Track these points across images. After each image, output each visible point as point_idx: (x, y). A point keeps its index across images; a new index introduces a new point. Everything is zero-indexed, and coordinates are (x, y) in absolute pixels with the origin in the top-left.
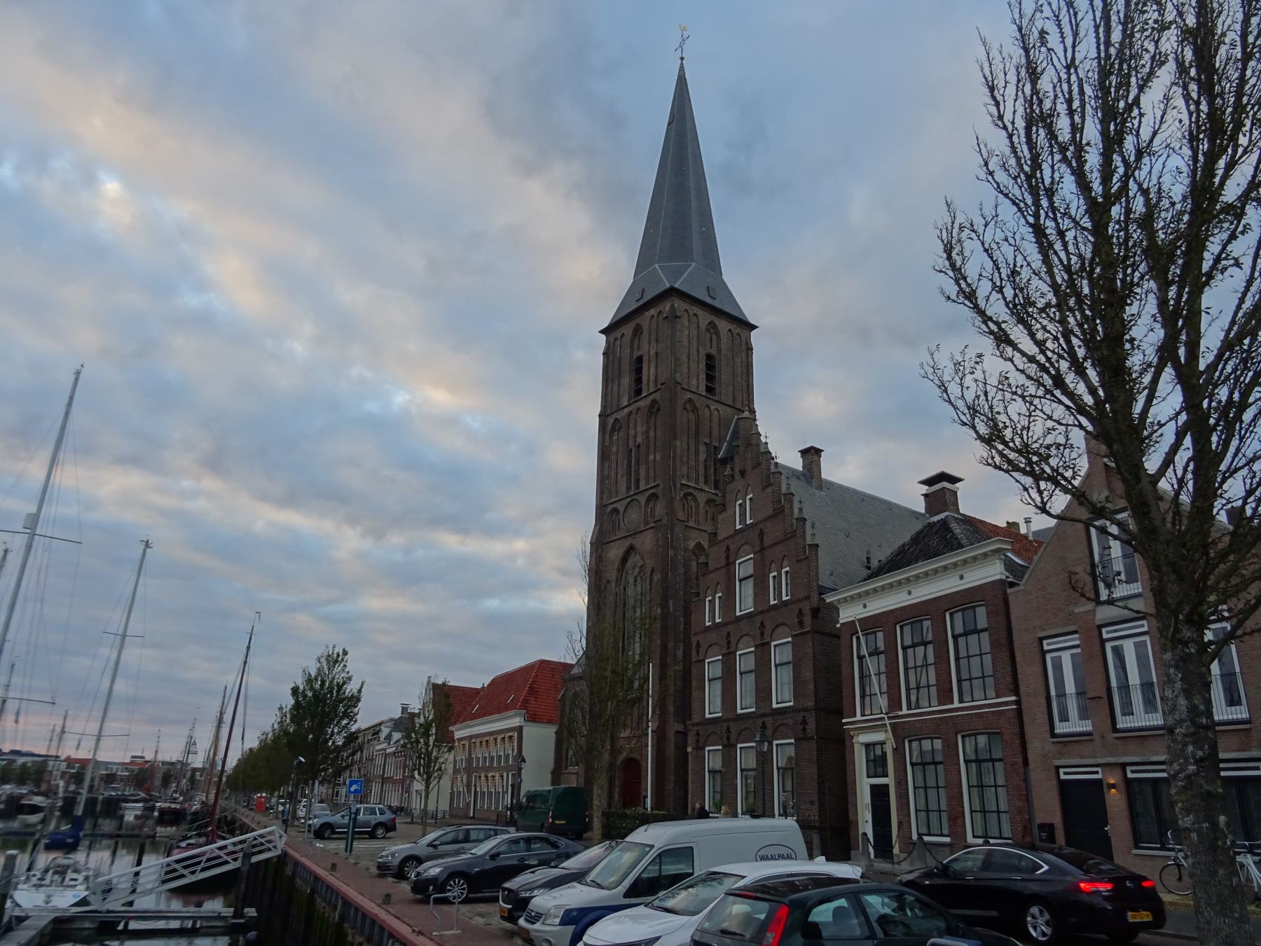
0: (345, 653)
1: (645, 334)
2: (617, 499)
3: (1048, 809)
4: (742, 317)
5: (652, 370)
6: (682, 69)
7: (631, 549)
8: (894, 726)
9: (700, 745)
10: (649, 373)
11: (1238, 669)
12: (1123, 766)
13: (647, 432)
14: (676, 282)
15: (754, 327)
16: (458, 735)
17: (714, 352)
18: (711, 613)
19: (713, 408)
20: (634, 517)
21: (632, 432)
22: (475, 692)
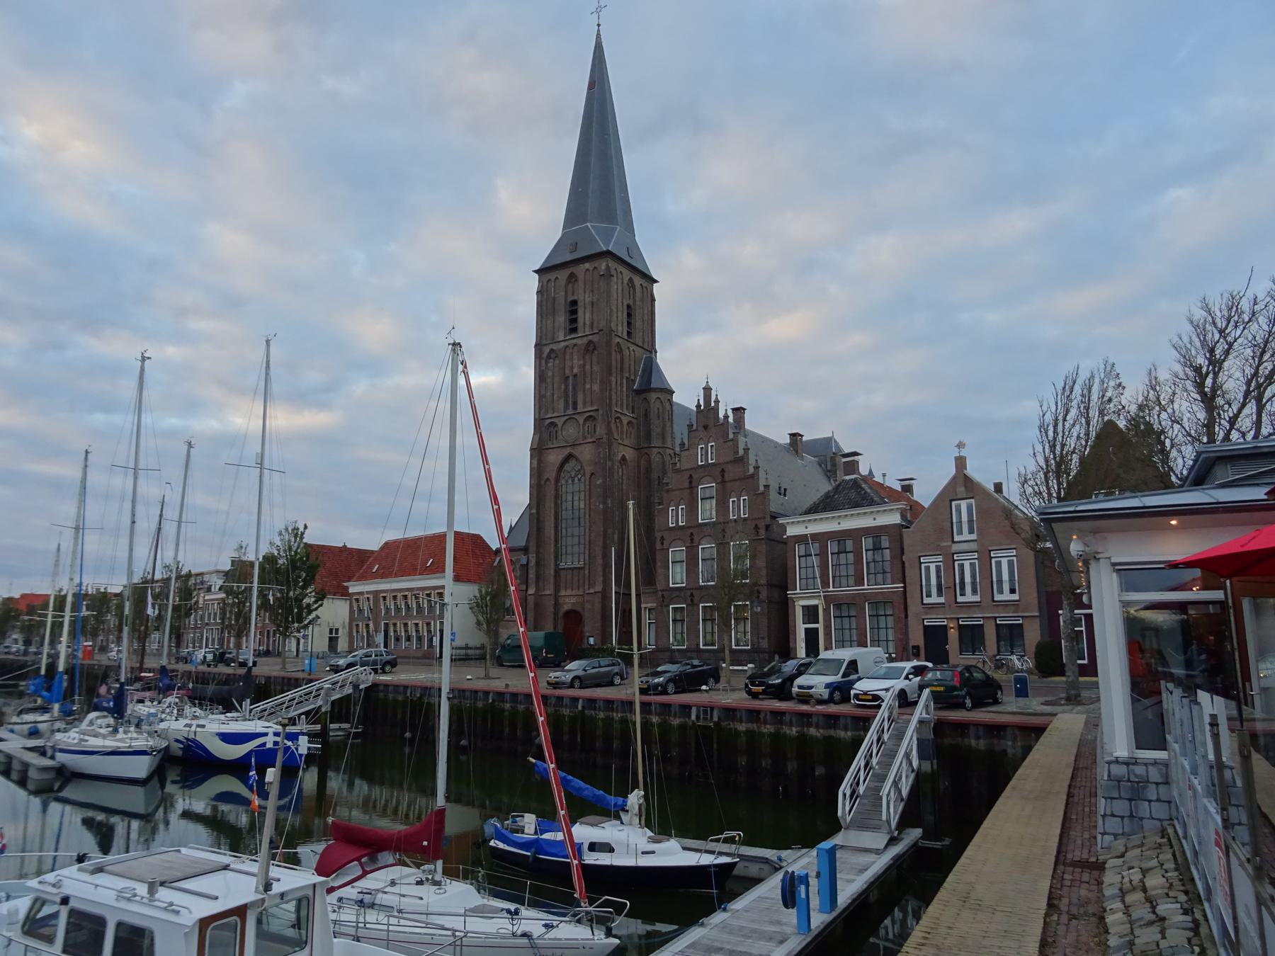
0: (306, 527)
1: (581, 283)
2: (554, 415)
3: (917, 638)
4: (646, 272)
5: (588, 315)
6: (598, 35)
7: (570, 456)
8: (825, 596)
10: (584, 316)
11: (1016, 578)
12: (958, 619)
13: (584, 366)
14: (609, 245)
15: (656, 281)
16: (351, 590)
17: (631, 302)
18: (675, 516)
19: (631, 349)
20: (571, 432)
21: (568, 363)
22: (372, 552)
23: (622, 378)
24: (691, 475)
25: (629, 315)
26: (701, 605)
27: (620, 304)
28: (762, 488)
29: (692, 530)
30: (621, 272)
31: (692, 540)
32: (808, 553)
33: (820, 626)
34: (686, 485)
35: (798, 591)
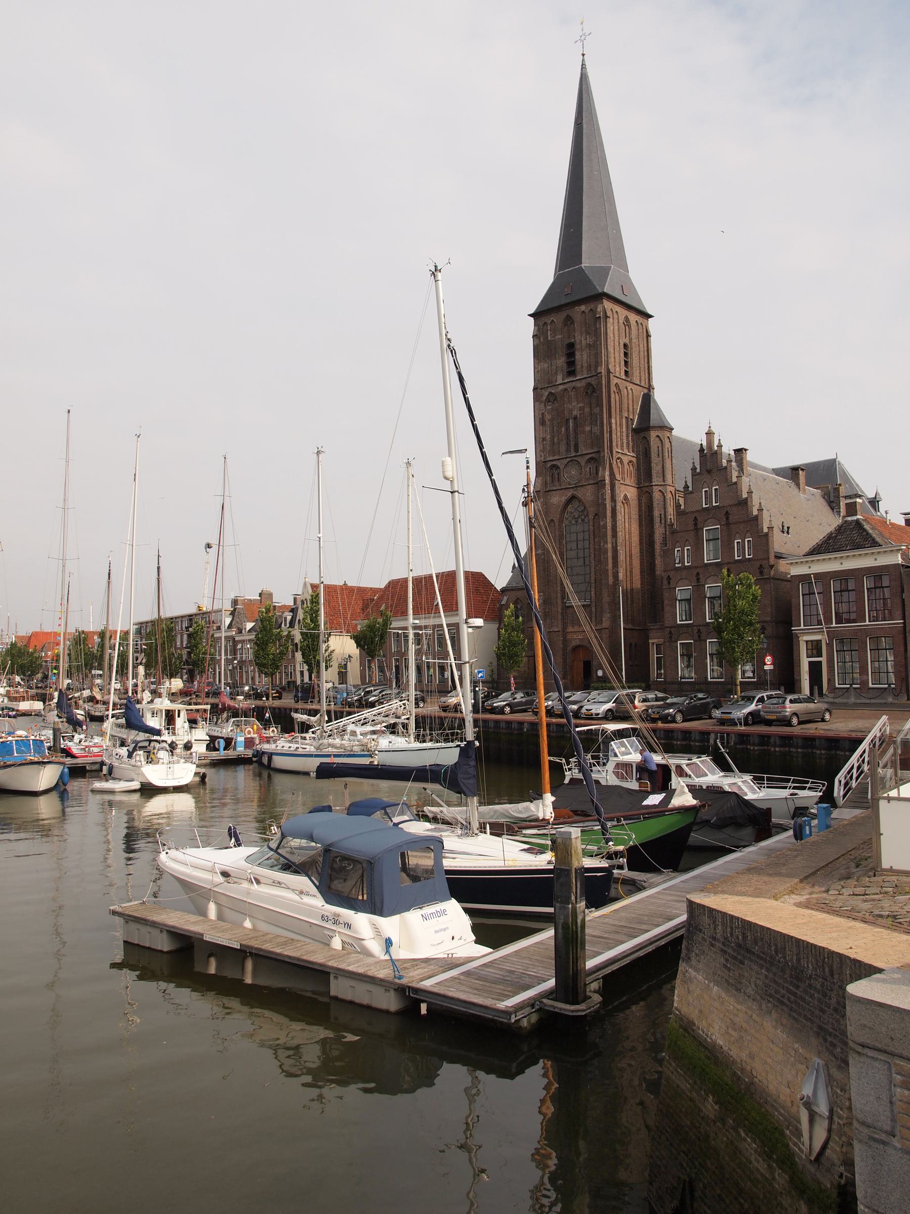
6: (583, 66)
7: (573, 498)
9: (673, 639)
15: (651, 316)
17: (627, 341)
19: (629, 388)
23: (621, 418)
24: (695, 517)
25: (626, 354)
26: (708, 641)
27: (617, 344)
28: (765, 530)
29: (699, 570)
30: (617, 312)
31: (698, 579)
32: (811, 592)
33: (823, 659)
34: (691, 527)
35: (802, 627)
